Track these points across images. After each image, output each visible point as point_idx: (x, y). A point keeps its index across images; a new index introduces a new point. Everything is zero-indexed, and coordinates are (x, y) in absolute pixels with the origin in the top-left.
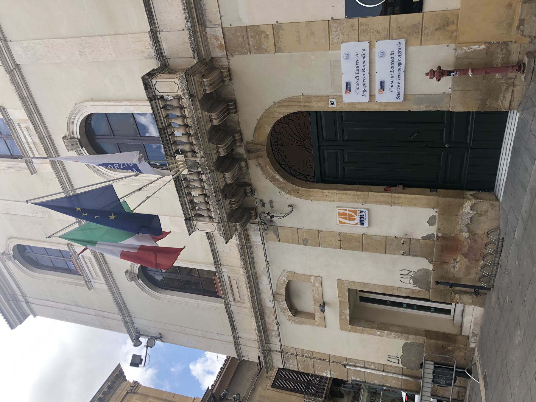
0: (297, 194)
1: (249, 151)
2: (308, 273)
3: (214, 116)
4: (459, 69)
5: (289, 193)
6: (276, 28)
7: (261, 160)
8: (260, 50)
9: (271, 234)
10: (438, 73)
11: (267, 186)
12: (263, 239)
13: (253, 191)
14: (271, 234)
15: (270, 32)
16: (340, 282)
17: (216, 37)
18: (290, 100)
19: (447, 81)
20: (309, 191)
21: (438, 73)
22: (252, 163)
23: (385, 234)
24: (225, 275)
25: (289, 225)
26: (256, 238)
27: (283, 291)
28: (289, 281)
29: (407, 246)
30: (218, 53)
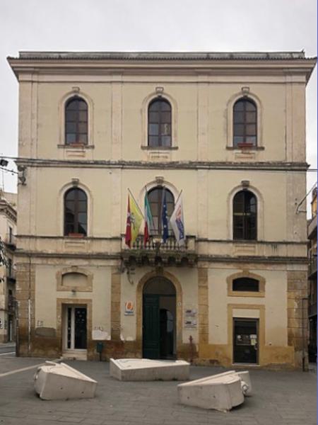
0: (139, 286)
1: (160, 268)
2: (93, 285)
3: (180, 260)
4: (192, 345)
5: (139, 282)
6: (207, 287)
7: (155, 273)
8: (200, 280)
9: (115, 271)
10: (191, 339)
11: (140, 274)
12: (112, 266)
13: (140, 266)
14: (115, 271)
15: (205, 285)
16: (91, 300)
17: (204, 265)
18: (181, 290)
19: (188, 341)
20: (175, 131)
21: (191, 339)
22: (154, 269)
23: (121, 320)
24: (85, 241)
25: (122, 280)
26: (112, 263)
27: (79, 271)
28: (86, 276)
29: (115, 332)
30: (200, 264)
